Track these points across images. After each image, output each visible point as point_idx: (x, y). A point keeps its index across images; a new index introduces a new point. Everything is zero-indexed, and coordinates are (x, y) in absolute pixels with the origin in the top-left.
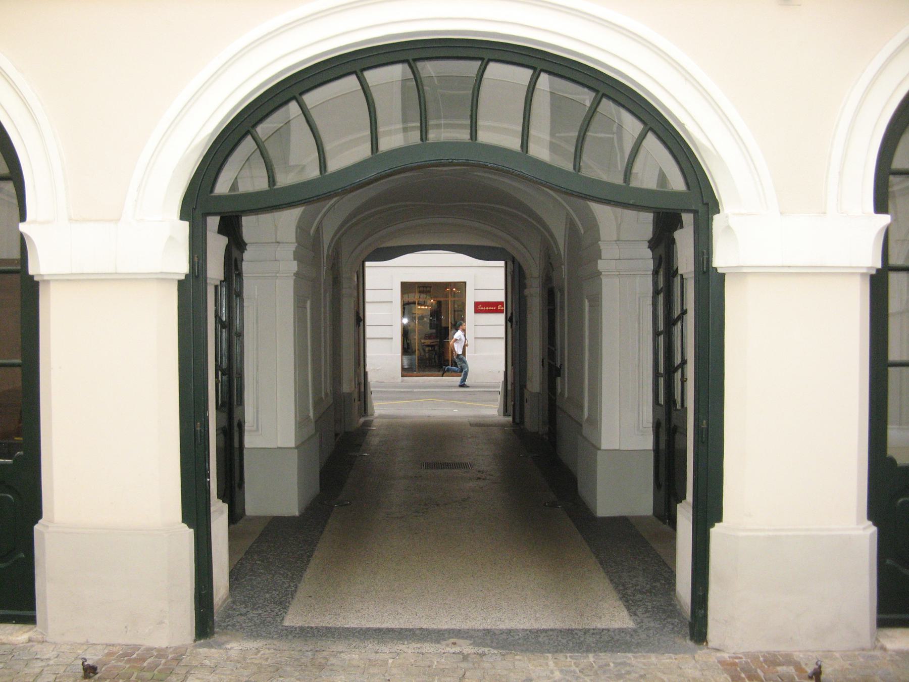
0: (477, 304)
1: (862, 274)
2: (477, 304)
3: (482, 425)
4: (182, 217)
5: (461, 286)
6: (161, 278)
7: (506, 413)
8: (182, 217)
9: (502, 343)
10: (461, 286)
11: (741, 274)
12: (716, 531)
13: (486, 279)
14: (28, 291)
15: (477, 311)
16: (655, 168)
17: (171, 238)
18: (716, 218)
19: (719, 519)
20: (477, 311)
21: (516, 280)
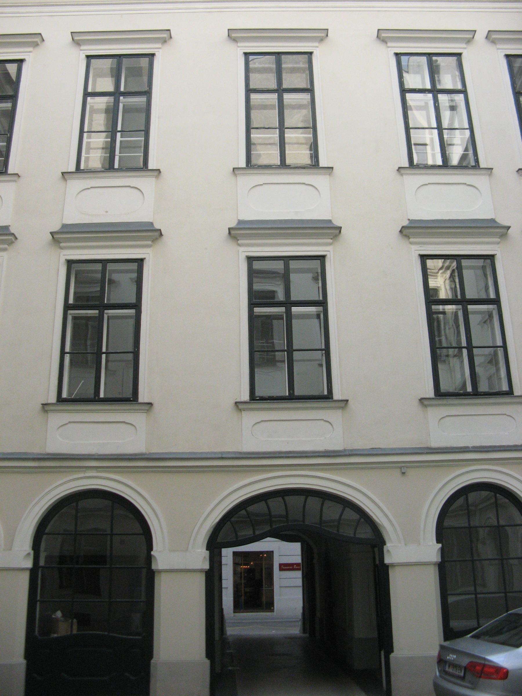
0: (280, 565)
1: (434, 564)
2: (280, 565)
3: (292, 638)
4: (207, 550)
5: (270, 554)
6: (201, 571)
7: (304, 631)
8: (207, 550)
9: (300, 591)
10: (270, 554)
11: (393, 565)
12: (392, 655)
13: (289, 552)
14: (151, 575)
15: (281, 569)
16: (364, 533)
17: (205, 557)
18: (385, 547)
19: (392, 651)
20: (281, 569)
21: (306, 553)
